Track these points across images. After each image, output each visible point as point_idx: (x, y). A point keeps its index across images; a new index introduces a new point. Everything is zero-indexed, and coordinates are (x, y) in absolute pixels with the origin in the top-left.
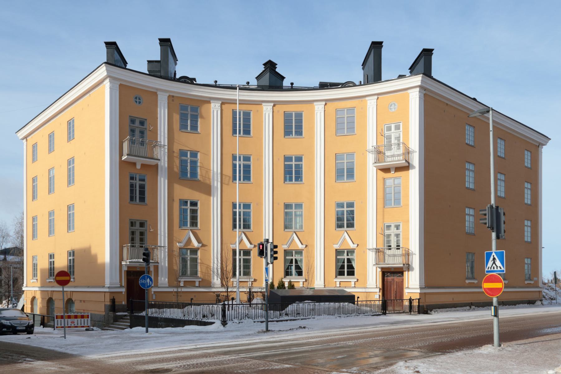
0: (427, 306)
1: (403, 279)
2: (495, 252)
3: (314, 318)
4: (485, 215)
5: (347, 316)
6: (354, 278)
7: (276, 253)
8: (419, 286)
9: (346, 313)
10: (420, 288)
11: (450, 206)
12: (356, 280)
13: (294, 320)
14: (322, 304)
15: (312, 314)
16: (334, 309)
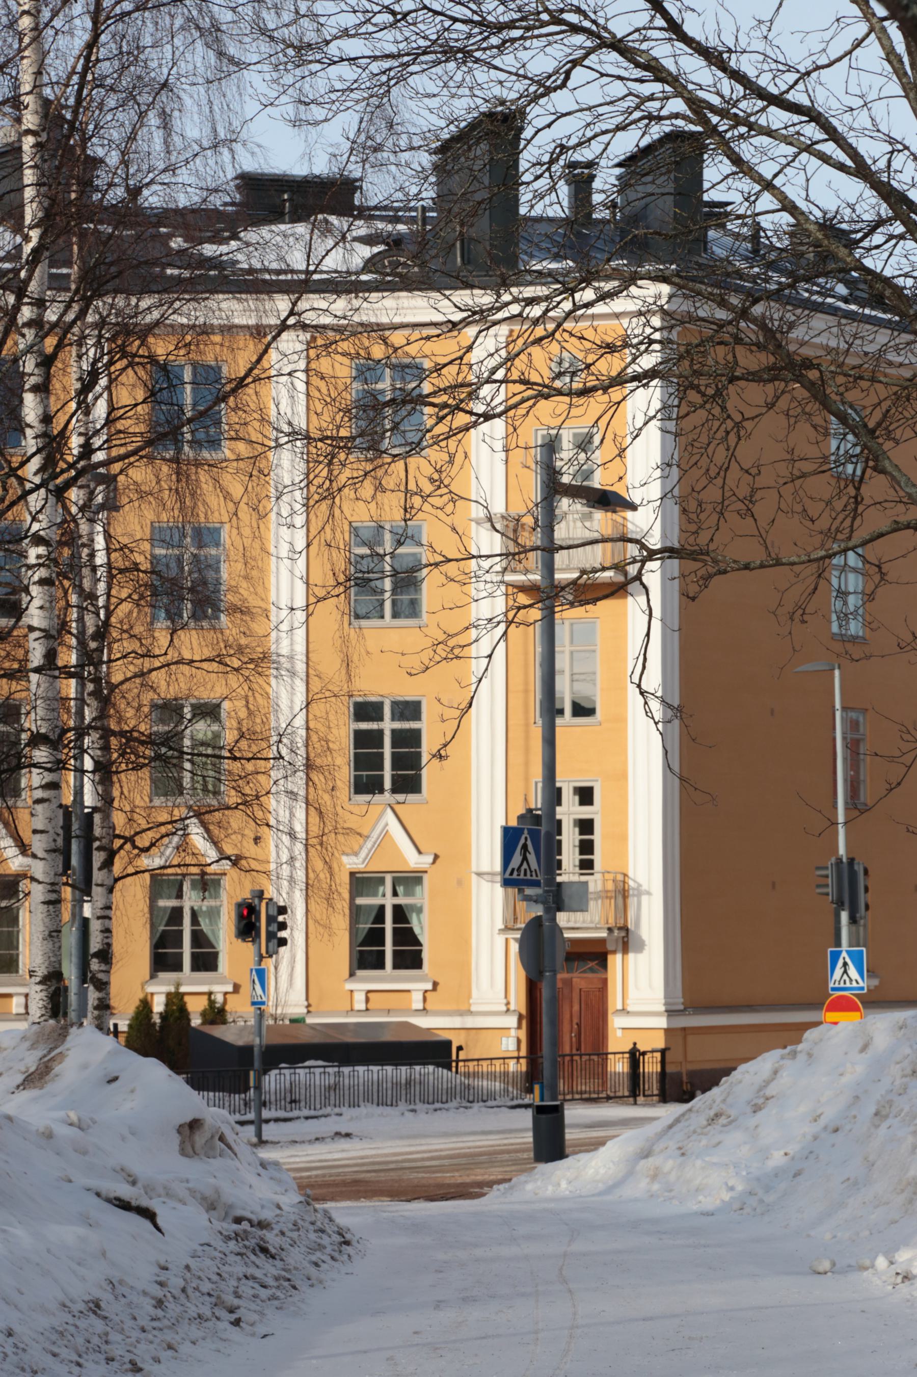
0: (692, 1074)
1: (605, 981)
2: (847, 952)
3: (341, 1115)
4: (827, 876)
5: (436, 1110)
6: (423, 979)
7: (283, 926)
8: (666, 1004)
9: (431, 1099)
10: (666, 1011)
11: (772, 712)
12: (429, 986)
13: (285, 1120)
14: (361, 1069)
15: (332, 1102)
16: (396, 1085)
